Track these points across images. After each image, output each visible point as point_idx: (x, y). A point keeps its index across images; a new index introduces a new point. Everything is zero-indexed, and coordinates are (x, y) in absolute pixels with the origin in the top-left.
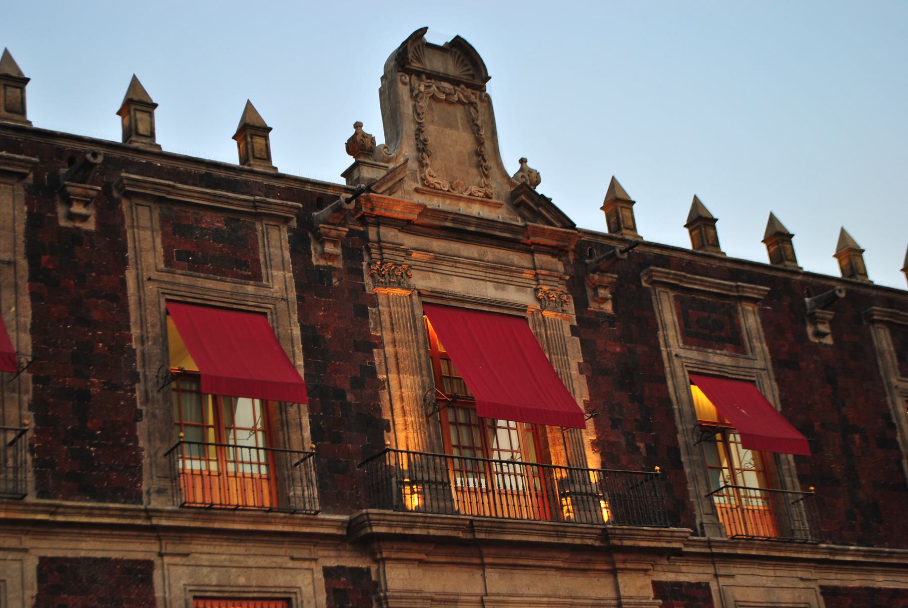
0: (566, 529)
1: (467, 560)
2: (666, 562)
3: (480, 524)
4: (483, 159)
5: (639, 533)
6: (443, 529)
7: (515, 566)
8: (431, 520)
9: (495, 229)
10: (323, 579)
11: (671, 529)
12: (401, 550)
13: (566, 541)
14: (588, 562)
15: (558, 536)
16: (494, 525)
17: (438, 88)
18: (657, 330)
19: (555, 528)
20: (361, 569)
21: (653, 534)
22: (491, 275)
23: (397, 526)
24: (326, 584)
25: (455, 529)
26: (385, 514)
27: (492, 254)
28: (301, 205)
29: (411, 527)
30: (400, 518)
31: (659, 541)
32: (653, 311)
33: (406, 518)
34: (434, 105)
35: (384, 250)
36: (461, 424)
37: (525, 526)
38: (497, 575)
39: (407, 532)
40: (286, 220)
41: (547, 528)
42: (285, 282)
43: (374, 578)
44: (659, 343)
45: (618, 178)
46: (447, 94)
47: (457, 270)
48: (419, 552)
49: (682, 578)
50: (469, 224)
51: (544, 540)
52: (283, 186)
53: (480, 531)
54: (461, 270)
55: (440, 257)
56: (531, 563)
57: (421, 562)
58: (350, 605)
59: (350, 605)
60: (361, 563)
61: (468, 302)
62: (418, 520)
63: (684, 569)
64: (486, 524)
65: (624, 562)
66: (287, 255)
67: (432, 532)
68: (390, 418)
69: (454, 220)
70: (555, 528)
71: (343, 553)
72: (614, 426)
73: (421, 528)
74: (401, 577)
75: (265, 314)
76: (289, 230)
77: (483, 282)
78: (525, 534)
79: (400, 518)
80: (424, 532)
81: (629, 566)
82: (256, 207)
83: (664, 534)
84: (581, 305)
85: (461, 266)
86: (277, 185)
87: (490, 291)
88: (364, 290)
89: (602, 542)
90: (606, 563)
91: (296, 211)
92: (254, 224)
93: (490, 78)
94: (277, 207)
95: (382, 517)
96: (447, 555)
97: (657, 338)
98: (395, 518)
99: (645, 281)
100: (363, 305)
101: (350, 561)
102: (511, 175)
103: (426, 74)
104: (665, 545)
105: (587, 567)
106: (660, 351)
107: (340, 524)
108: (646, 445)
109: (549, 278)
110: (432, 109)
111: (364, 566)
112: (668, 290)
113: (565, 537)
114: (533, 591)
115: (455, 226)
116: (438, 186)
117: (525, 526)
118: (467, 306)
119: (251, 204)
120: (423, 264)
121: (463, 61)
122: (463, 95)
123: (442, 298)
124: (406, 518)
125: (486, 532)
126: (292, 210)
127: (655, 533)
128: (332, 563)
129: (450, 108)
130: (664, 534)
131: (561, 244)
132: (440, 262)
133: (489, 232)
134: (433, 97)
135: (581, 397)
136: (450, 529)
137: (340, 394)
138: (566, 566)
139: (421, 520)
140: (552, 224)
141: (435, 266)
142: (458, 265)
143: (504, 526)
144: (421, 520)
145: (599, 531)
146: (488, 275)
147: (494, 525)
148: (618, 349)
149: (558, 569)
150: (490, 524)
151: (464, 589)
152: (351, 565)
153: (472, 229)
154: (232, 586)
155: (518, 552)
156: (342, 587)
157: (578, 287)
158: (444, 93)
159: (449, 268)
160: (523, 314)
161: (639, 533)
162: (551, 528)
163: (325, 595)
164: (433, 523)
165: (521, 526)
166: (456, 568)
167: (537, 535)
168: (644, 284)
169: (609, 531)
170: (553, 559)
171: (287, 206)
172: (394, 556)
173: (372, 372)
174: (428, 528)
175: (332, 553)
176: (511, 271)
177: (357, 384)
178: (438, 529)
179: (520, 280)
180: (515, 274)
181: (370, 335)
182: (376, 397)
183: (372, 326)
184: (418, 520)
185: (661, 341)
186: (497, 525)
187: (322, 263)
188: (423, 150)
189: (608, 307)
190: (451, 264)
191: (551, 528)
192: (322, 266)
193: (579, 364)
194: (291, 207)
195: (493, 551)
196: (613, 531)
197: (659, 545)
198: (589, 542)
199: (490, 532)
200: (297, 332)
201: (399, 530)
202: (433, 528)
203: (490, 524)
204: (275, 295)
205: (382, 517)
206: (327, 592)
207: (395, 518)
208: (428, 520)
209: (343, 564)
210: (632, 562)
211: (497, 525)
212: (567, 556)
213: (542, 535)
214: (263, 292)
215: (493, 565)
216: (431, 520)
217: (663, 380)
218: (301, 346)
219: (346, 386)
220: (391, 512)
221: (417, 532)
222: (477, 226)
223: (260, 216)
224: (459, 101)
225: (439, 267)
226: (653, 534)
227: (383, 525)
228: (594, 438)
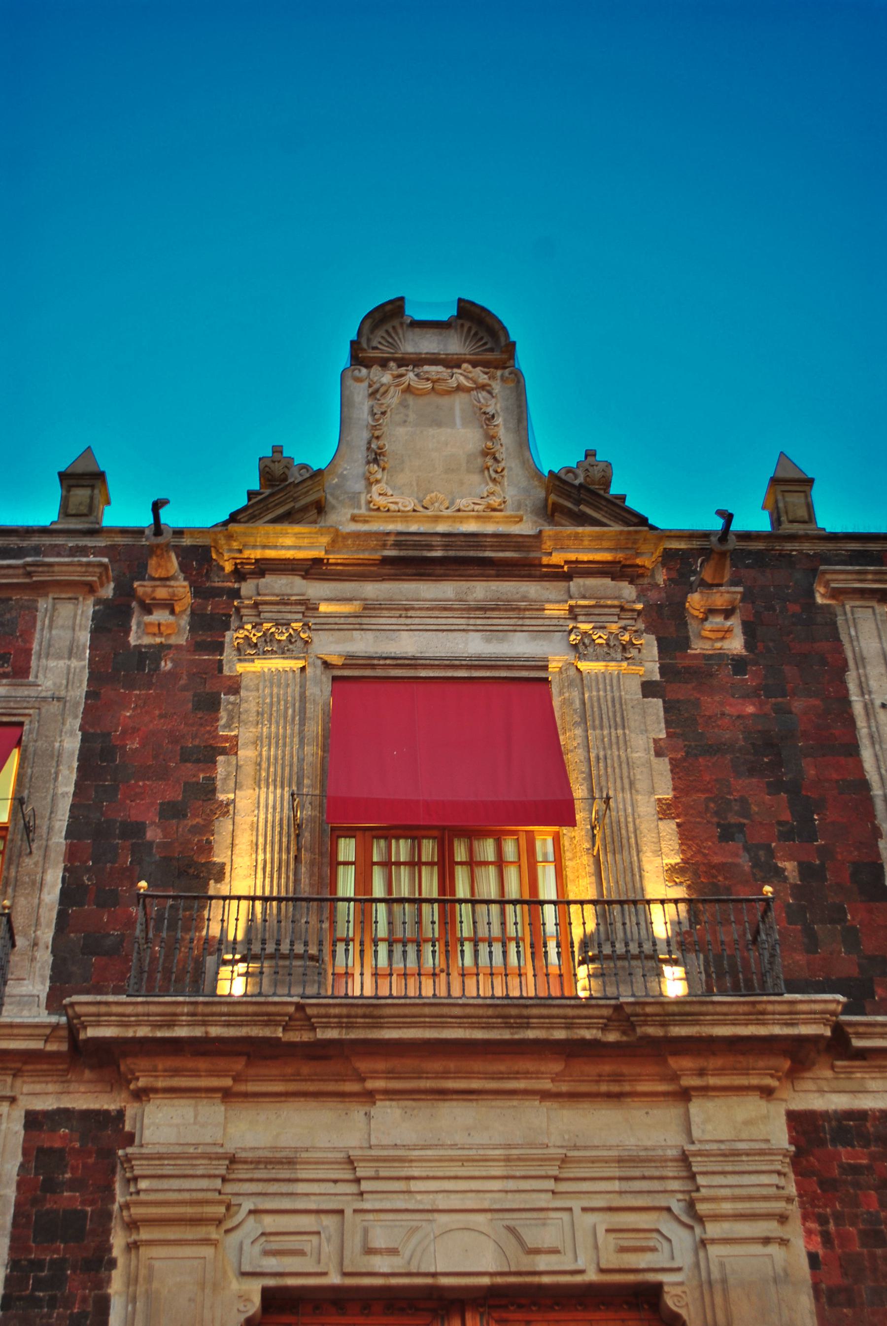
0: (526, 1012)
1: (331, 1087)
2: (829, 1074)
3: (322, 1011)
4: (496, 460)
5: (704, 1009)
6: (240, 1024)
7: (443, 1094)
8: (208, 1010)
9: (483, 547)
10: (23, 1132)
11: (788, 997)
12: (176, 1072)
13: (531, 1034)
14: (617, 1078)
15: (509, 1026)
16: (354, 1011)
17: (417, 375)
18: (845, 668)
19: (499, 1011)
20: (107, 1112)
21: (742, 1009)
22: (479, 622)
23: (138, 1024)
24: (25, 1140)
25: (267, 1024)
26: (107, 1003)
27: (480, 590)
28: (105, 560)
29: (171, 1025)
30: (140, 1009)
31: (764, 1023)
32: (839, 640)
33: (153, 1009)
34: (410, 400)
35: (261, 608)
36: (398, 864)
37: (427, 1011)
38: (398, 1112)
39: (159, 1034)
40: (91, 588)
41: (480, 1012)
42: (68, 674)
43: (127, 1128)
44: (847, 690)
45: (788, 453)
46: (434, 382)
47: (409, 621)
48: (212, 1073)
49: (866, 1103)
50: (430, 547)
51: (479, 1035)
52: (103, 545)
53: (326, 1026)
54: (417, 621)
55: (370, 608)
56: (475, 1085)
57: (227, 1095)
58: (68, 1175)
59: (68, 1175)
60: (108, 1103)
61: (425, 667)
62: (179, 1010)
63: (873, 1085)
64: (336, 1011)
65: (702, 1073)
66: (85, 637)
67: (215, 1031)
68: (227, 860)
69: (398, 545)
70: (499, 1011)
71: (73, 1087)
72: (727, 834)
73: (190, 1024)
74: (175, 1121)
75: (21, 724)
76: (98, 602)
77: (463, 634)
78: (431, 1026)
79: (140, 1009)
80: (198, 1032)
81: (712, 1081)
82: (29, 574)
83: (770, 1008)
84: (673, 643)
85: (418, 613)
86: (90, 544)
87: (474, 645)
88: (221, 670)
89: (624, 1033)
90: (663, 1079)
91: (97, 570)
92: (37, 601)
93: (63, 476)
94: (64, 568)
95: (103, 1009)
96: (285, 1079)
97: (843, 684)
98: (129, 1009)
99: (823, 596)
100: (211, 692)
101: (85, 1098)
102: (732, 528)
103: (395, 360)
104: (777, 1030)
105: (615, 1088)
106: (849, 703)
107: (48, 1031)
108: (800, 864)
109: (597, 611)
110: (406, 407)
111: (112, 1107)
112: (874, 604)
113: (528, 1026)
114: (479, 1138)
115: (403, 553)
116: (393, 507)
117: (427, 1011)
118: (423, 673)
119: (21, 571)
120: (342, 620)
121: (476, 334)
122: (466, 377)
123: (373, 667)
124: (153, 1009)
125: (340, 1026)
126: (91, 569)
127: (746, 1008)
128: (47, 1103)
129: (445, 401)
130: (770, 1008)
131: (620, 556)
132: (373, 613)
133: (472, 554)
134: (409, 389)
135: (653, 791)
136: (255, 1023)
137: (135, 830)
138: (564, 1088)
139: (186, 1009)
140: (605, 525)
141: (365, 620)
142: (410, 613)
143: (377, 1012)
144: (186, 1009)
145: (605, 1012)
146: (472, 621)
147: (354, 1011)
148: (750, 709)
149: (545, 1095)
150: (344, 1011)
151: (322, 1140)
152: (84, 1107)
153: (438, 554)
154: (702, 1294)
155: (437, 1065)
156: (57, 1145)
157: (668, 623)
158: (428, 379)
159: (393, 621)
160: (541, 674)
161: (704, 1009)
162: (490, 1012)
163: (20, 1159)
164: (213, 1015)
165: (415, 1011)
166: (312, 1104)
167: (460, 1026)
168: (819, 600)
169: (628, 1010)
170: (526, 1075)
171: (81, 564)
172: (160, 1083)
173: (209, 789)
174: (205, 1024)
175: (51, 1088)
176: (519, 609)
177: (172, 811)
178: (228, 1024)
179: (540, 622)
180: (528, 614)
181: (216, 737)
182: (207, 828)
183: (222, 722)
184: (179, 1010)
185: (852, 687)
186: (360, 1011)
187: (147, 640)
188: (376, 461)
189: (736, 645)
190: (397, 613)
191: (490, 1012)
192: (145, 646)
193: (656, 741)
194: (88, 564)
195: (381, 1065)
196: (638, 1009)
197: (762, 1031)
198: (588, 1034)
199: (349, 1026)
200: (71, 744)
201: (143, 1032)
202: (215, 1024)
203: (344, 1011)
204: (44, 694)
205: (103, 1009)
206: (25, 1152)
207: (129, 1009)
208: (200, 1009)
209: (69, 1106)
210: (720, 1072)
211: (360, 1011)
212: (557, 1067)
213: (472, 1026)
214: (32, 692)
215: (390, 1094)
216: (208, 1010)
217: (852, 749)
218: (75, 764)
219: (151, 816)
220: (123, 998)
221: (181, 1032)
222: (446, 547)
223: (41, 588)
224: (459, 388)
225: (373, 621)
226: (742, 1009)
227: (109, 1025)
228: (676, 859)
